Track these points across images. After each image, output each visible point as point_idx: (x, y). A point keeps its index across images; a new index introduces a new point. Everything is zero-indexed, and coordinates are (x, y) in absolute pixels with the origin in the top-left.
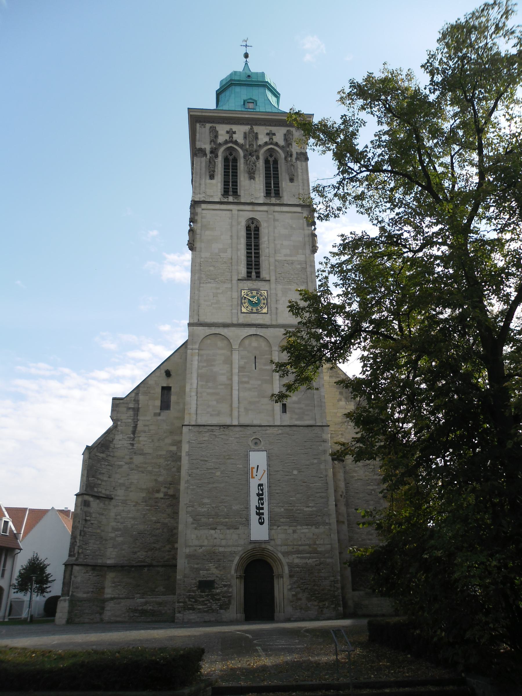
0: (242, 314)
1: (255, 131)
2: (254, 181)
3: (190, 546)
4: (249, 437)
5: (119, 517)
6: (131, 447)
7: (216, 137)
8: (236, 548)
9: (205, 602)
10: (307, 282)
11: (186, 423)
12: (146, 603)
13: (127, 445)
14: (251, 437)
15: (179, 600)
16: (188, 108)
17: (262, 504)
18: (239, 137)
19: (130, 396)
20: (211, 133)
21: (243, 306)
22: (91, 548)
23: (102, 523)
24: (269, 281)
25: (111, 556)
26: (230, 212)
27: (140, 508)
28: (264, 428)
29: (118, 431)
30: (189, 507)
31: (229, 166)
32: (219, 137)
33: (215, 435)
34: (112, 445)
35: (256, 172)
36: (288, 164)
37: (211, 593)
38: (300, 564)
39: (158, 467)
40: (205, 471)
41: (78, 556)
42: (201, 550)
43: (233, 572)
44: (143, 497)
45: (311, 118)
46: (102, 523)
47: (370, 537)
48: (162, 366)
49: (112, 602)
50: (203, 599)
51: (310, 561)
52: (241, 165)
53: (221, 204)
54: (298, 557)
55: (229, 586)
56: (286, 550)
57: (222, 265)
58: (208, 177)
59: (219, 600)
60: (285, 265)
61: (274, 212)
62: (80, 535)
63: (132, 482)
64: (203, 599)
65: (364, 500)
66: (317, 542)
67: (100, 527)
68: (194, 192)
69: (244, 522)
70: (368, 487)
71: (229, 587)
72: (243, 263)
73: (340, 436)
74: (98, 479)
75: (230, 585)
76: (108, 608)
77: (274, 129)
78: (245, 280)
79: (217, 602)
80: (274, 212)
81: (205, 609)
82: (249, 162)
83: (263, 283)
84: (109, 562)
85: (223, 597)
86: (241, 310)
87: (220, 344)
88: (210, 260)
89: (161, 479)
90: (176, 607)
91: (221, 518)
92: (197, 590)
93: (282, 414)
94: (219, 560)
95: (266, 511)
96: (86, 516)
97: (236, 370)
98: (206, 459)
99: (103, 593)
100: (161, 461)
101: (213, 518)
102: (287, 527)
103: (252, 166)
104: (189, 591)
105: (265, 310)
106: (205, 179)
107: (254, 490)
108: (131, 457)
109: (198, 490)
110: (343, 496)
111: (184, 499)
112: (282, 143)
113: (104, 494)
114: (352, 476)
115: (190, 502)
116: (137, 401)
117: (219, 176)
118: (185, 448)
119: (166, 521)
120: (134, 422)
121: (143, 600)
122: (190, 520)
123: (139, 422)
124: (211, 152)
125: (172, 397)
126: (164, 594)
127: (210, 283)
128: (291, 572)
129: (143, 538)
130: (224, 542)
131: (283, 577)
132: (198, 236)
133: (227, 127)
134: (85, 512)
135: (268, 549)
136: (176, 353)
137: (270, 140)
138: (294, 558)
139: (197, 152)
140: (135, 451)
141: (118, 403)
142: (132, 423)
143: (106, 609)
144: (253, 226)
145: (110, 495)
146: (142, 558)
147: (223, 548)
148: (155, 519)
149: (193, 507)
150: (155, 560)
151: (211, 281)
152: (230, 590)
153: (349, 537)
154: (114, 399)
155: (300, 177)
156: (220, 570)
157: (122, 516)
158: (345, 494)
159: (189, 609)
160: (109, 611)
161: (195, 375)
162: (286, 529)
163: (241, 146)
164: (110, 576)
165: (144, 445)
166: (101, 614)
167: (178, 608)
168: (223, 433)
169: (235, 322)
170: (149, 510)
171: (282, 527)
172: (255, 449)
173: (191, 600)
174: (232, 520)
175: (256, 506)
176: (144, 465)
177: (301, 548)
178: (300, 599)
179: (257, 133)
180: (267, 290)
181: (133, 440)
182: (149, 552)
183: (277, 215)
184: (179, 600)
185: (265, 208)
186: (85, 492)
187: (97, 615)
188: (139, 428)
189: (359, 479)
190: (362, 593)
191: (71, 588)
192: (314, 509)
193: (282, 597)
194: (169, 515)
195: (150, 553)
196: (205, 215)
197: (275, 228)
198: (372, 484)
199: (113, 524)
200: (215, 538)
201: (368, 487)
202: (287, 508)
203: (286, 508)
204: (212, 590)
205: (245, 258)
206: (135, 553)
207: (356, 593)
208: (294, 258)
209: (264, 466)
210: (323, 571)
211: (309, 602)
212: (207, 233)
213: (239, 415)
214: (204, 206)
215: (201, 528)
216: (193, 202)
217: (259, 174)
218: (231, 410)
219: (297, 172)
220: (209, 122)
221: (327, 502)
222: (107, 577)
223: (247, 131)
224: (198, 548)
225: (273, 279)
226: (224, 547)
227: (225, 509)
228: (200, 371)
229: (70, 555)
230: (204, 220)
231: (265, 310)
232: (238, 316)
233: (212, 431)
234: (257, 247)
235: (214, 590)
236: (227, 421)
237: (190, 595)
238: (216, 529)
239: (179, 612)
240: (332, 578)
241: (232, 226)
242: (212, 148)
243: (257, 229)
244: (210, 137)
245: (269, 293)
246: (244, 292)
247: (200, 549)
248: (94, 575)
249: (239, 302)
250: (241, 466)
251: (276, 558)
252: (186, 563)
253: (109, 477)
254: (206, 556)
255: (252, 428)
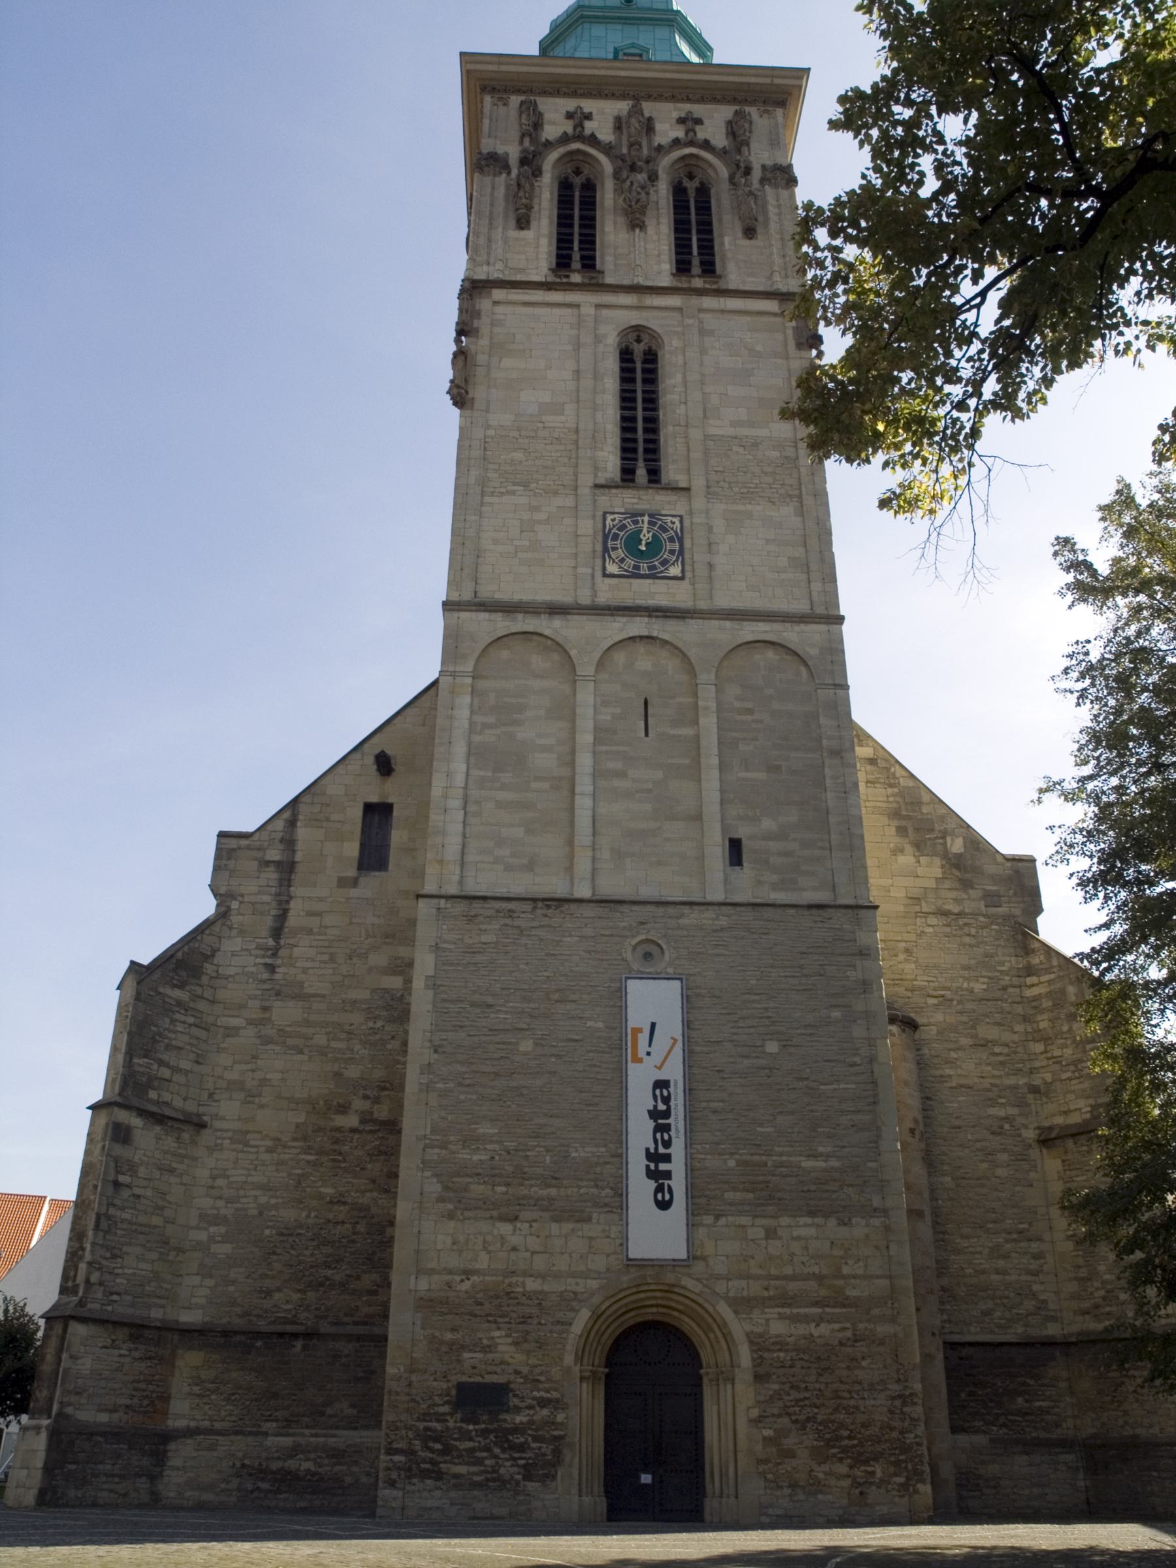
0: (608, 581)
1: (647, 115)
2: (642, 235)
3: (431, 1272)
4: (627, 937)
5: (220, 1182)
6: (266, 976)
7: (537, 125)
8: (581, 1281)
9: (478, 1454)
10: (800, 496)
11: (430, 888)
12: (294, 1451)
13: (254, 969)
14: (634, 936)
15: (390, 1443)
16: (462, 54)
17: (667, 1144)
18: (601, 126)
19: (269, 827)
20: (524, 116)
21: (610, 557)
22: (130, 1271)
23: (168, 1197)
24: (687, 489)
25: (194, 1300)
26: (575, 310)
27: (287, 1156)
28: (671, 910)
29: (231, 928)
30: (433, 1147)
31: (572, 217)
32: (546, 127)
33: (519, 927)
34: (209, 968)
35: (650, 212)
36: (740, 192)
37: (495, 1425)
38: (788, 1340)
39: (344, 1036)
40: (483, 1038)
41: (84, 1293)
42: (466, 1285)
43: (569, 1359)
44: (298, 1126)
45: (802, 78)
46: (168, 1197)
47: (1001, 1263)
48: (366, 746)
49: (189, 1441)
50: (470, 1444)
51: (824, 1329)
52: (607, 196)
53: (550, 289)
54: (781, 1317)
55: (556, 1404)
56: (745, 1294)
57: (549, 447)
58: (512, 223)
59: (522, 1448)
60: (735, 448)
61: (701, 310)
62: (97, 1227)
63: (265, 1079)
64: (470, 1444)
65: (978, 1150)
66: (846, 1270)
67: (162, 1208)
68: (472, 260)
69: (606, 1200)
70: (992, 1111)
71: (556, 1409)
72: (610, 441)
73: (902, 957)
74: (161, 1063)
75: (557, 1401)
76: (175, 1461)
77: (698, 110)
78: (617, 487)
79: (516, 1455)
80: (701, 310)
81: (476, 1478)
82: (628, 183)
83: (671, 497)
84: (189, 1318)
85: (536, 1439)
86: (604, 568)
87: (538, 661)
88: (516, 434)
89: (353, 1072)
90: (382, 1465)
91: (532, 1186)
92: (452, 1414)
93: (729, 869)
94: (525, 1320)
95: (677, 1167)
96: (118, 1172)
97: (585, 738)
98: (490, 1000)
99: (165, 1413)
100: (357, 1018)
101: (508, 1185)
102: (745, 1220)
103: (639, 193)
104: (425, 1417)
105: (675, 571)
106: (505, 229)
107: (640, 1100)
108: (267, 1004)
109: (462, 1097)
110: (917, 1133)
111: (414, 1125)
112: (720, 140)
113: (176, 1110)
114: (942, 1076)
115: (433, 1132)
116: (289, 843)
117: (545, 222)
118: (425, 964)
119: (365, 1200)
120: (280, 902)
121: (287, 1441)
122: (434, 1187)
123: (292, 904)
124: (524, 161)
125: (393, 832)
126: (352, 1425)
127: (513, 493)
128: (760, 1365)
129: (292, 1247)
130: (539, 1263)
131: (733, 1381)
132: (480, 372)
133: (570, 104)
134: (116, 1160)
135: (684, 1288)
136: (409, 711)
137: (686, 134)
138: (767, 1320)
139: (483, 163)
140: (277, 987)
141: (235, 846)
142: (274, 904)
143: (170, 1463)
144: (638, 350)
145: (198, 1115)
146: (290, 1310)
147: (539, 1281)
148: (329, 1191)
149: (444, 1146)
150: (326, 1317)
151: (516, 488)
152: (560, 1417)
153: (938, 1262)
154: (222, 835)
155: (773, 226)
156: (528, 1353)
157: (231, 1179)
158: (921, 1127)
159: (424, 1475)
160: (178, 1469)
161: (460, 749)
162: (744, 1226)
163: (607, 149)
164: (190, 1360)
165: (305, 971)
166: (153, 1478)
167: (388, 1469)
168: (546, 921)
169: (585, 599)
170: (315, 1164)
171: (731, 1219)
172: (642, 973)
173: (431, 1444)
174: (569, 1192)
175: (647, 1150)
176: (304, 1030)
177: (792, 1287)
178: (792, 1454)
179: (650, 119)
180: (681, 517)
181: (274, 955)
182: (309, 1294)
183: (709, 320)
184: (390, 1443)
185: (674, 301)
186: (119, 1099)
187: (143, 1483)
188: (292, 921)
189: (961, 1086)
190: (980, 1440)
191: (58, 1393)
192: (834, 1163)
193: (731, 1447)
194: (374, 1181)
195: (311, 1295)
196: (502, 317)
197: (703, 351)
198: (1003, 1101)
199: (206, 1203)
200: (514, 1249)
201: (992, 1111)
202: (749, 1157)
203: (744, 1157)
204: (501, 1417)
205: (617, 431)
206: (268, 1293)
207: (963, 1439)
208: (763, 432)
209: (671, 1026)
210: (864, 1363)
211: (819, 1464)
212: (507, 362)
213: (594, 869)
214: (498, 294)
215: (467, 1214)
216: (467, 284)
217: (658, 219)
218: (571, 857)
219: (765, 212)
220: (518, 91)
221: (876, 1142)
222: (179, 1363)
223: (625, 113)
224: (458, 1278)
225: (698, 483)
226: (543, 1277)
227: (548, 1158)
228: (477, 738)
229: (63, 1290)
230: (497, 330)
231: (675, 571)
232: (593, 584)
233: (510, 914)
234: (651, 402)
235: (508, 1417)
236: (556, 886)
237: (427, 1429)
238: (516, 1218)
239: (392, 1484)
240: (895, 1388)
241: (578, 346)
242: (524, 151)
243: (651, 357)
244: (521, 125)
245: (687, 523)
246: (613, 520)
247: (462, 1281)
248: (136, 1354)
249: (599, 547)
250: (600, 1025)
251: (710, 1320)
252: (418, 1322)
253: (197, 1062)
254: (481, 1304)
255: (635, 908)
